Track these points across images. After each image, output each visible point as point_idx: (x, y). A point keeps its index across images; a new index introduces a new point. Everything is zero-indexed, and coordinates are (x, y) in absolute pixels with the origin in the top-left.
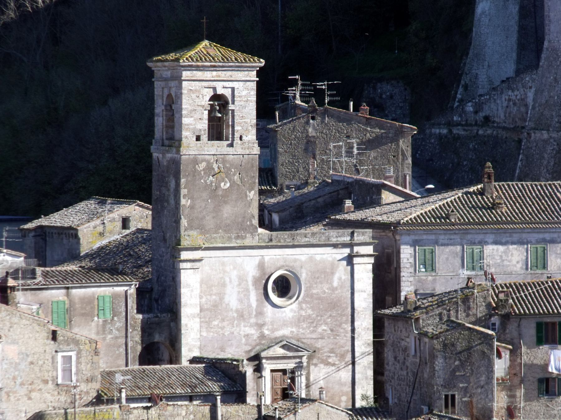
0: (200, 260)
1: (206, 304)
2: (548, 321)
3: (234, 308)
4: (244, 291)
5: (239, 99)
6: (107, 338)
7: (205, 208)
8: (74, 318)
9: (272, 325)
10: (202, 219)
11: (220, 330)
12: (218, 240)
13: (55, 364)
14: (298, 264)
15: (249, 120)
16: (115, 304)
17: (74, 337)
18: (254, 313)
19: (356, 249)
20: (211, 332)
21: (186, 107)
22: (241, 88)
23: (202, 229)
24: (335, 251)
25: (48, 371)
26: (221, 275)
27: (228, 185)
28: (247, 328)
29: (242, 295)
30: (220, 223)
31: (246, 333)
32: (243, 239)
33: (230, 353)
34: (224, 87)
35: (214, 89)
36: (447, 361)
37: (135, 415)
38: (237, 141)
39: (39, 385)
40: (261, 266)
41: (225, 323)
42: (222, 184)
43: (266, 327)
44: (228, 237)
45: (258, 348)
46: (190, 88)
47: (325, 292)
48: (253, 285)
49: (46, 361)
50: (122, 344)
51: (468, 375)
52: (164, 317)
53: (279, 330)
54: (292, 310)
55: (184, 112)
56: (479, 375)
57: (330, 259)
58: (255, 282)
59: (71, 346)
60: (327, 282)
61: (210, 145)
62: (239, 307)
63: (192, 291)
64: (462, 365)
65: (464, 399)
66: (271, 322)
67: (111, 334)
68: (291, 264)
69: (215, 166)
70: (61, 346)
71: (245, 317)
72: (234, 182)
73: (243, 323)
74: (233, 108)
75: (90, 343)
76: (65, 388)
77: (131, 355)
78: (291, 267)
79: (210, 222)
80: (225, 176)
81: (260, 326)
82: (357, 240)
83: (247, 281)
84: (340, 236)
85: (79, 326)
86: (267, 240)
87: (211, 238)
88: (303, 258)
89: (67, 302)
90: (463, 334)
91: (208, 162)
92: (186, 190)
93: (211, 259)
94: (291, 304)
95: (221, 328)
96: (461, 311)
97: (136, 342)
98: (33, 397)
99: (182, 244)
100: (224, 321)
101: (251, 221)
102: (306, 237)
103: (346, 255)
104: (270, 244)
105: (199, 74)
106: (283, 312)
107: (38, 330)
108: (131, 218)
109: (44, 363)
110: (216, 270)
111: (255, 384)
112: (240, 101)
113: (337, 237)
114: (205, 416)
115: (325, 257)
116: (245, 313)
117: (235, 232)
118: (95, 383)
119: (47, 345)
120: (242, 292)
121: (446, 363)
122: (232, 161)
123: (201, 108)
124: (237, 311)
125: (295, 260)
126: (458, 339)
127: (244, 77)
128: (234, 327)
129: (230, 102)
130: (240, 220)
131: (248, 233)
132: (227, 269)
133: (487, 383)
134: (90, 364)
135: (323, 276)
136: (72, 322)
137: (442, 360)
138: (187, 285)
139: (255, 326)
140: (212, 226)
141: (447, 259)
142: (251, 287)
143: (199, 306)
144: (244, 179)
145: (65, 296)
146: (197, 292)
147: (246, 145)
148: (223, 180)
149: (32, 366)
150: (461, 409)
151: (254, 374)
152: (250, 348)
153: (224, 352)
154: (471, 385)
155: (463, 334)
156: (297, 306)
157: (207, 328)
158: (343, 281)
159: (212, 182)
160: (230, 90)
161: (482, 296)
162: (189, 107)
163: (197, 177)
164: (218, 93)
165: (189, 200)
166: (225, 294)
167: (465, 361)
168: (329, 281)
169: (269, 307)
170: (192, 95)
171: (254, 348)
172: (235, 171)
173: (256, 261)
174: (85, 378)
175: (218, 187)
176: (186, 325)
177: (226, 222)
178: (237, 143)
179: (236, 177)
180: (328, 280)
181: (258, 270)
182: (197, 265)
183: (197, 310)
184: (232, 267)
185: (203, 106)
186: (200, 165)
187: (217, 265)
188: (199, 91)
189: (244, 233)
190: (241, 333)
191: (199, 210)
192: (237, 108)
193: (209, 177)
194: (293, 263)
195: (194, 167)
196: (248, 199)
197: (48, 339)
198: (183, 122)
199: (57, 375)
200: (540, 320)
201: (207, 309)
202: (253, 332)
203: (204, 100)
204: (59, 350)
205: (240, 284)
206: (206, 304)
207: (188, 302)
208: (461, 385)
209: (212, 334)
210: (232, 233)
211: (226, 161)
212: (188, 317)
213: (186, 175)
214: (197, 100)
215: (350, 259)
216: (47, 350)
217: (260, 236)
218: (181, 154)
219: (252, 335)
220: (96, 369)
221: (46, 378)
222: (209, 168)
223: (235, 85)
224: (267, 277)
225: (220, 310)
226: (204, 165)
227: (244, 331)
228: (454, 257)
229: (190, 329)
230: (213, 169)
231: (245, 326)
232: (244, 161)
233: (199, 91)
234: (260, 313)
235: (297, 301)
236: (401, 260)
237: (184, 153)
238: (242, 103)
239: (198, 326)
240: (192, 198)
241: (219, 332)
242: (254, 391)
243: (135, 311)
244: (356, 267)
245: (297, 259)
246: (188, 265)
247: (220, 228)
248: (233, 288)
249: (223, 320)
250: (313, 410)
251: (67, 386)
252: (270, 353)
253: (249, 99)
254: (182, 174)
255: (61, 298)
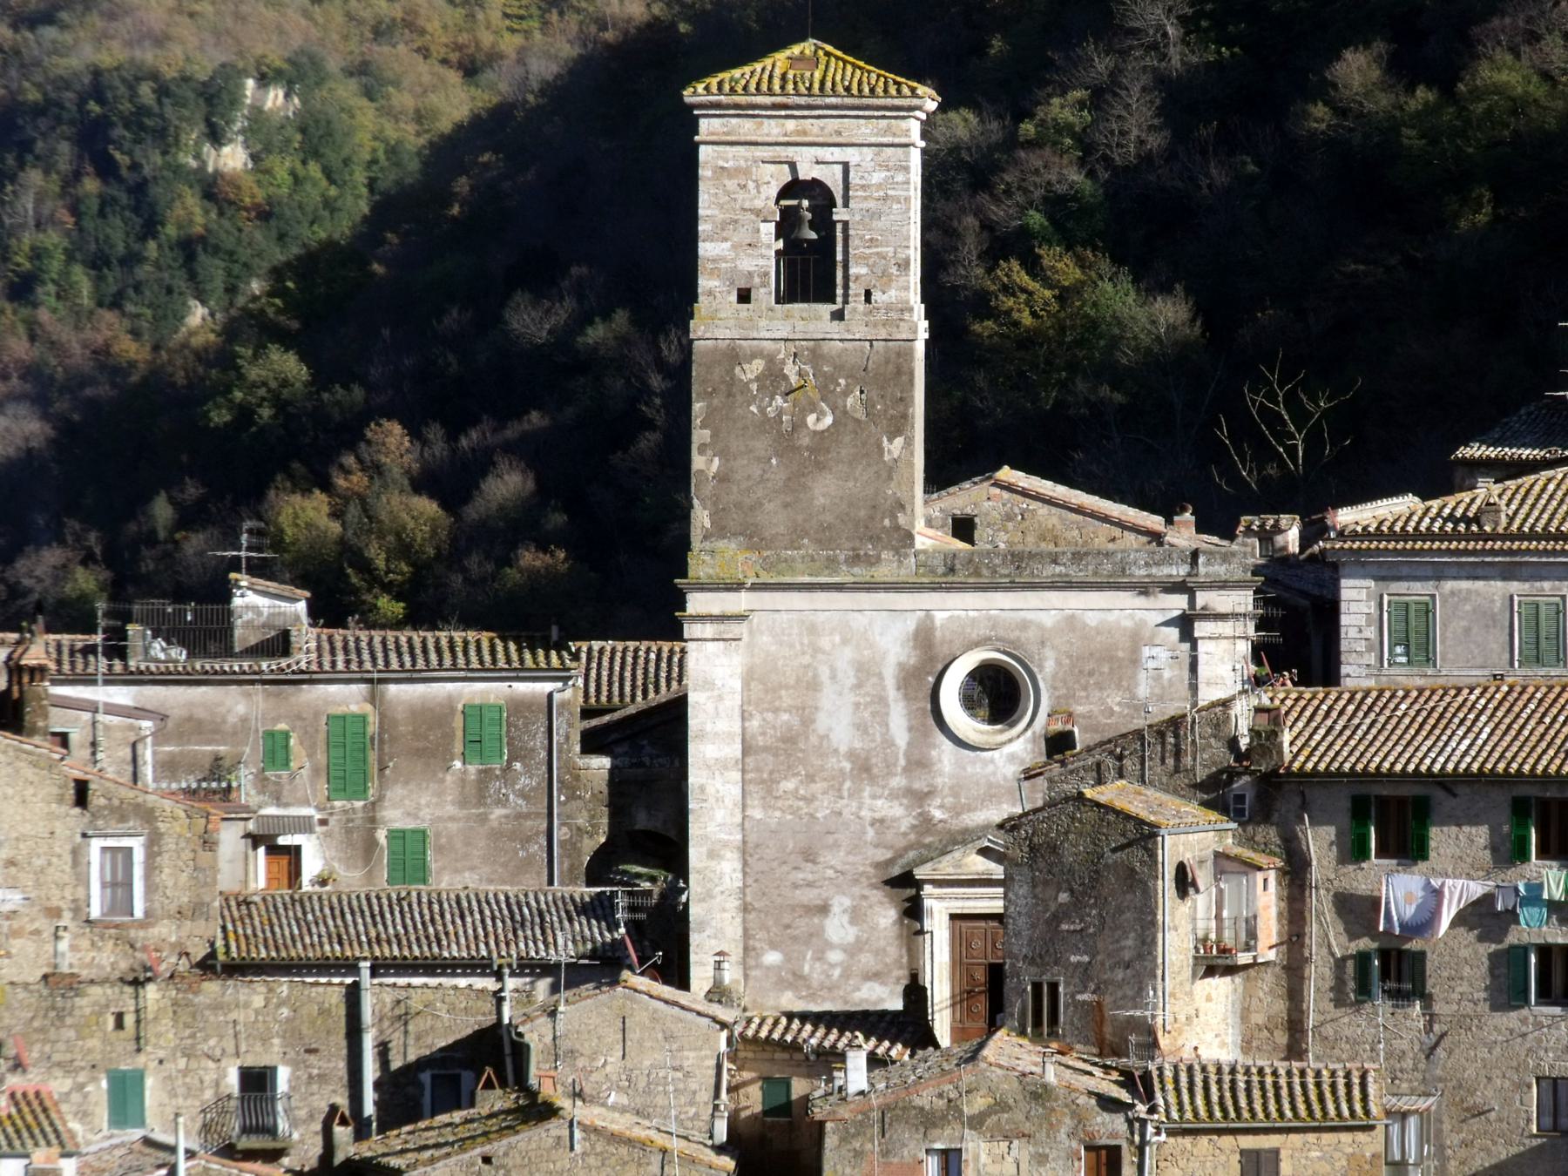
0: (740, 618)
1: (764, 734)
2: (1385, 793)
3: (843, 749)
4: (872, 702)
5: (860, 193)
6: (492, 817)
7: (762, 480)
8: (391, 759)
9: (956, 795)
10: (752, 508)
11: (801, 803)
12: (799, 566)
13: (82, 868)
14: (1032, 634)
15: (891, 249)
16: (516, 726)
17: (140, 800)
18: (902, 762)
19: (1202, 598)
20: (774, 808)
21: (709, 212)
22: (868, 165)
23: (754, 538)
24: (1141, 601)
25: (62, 886)
26: (806, 659)
27: (828, 420)
28: (879, 803)
29: (867, 715)
30: (805, 521)
31: (877, 815)
32: (872, 564)
33: (832, 867)
34: (818, 163)
35: (793, 166)
36: (1038, 890)
37: (92, 999)
38: (857, 304)
39: (32, 921)
40: (924, 638)
41: (818, 787)
42: (811, 419)
43: (938, 801)
44: (828, 558)
45: (912, 854)
46: (721, 163)
47: (1112, 713)
48: (899, 689)
49: (55, 860)
50: (537, 834)
51: (1091, 930)
52: (661, 766)
53: (975, 809)
54: (1012, 758)
55: (703, 227)
56: (1119, 932)
57: (1128, 623)
58: (904, 679)
59: (131, 824)
60: (1119, 686)
61: (779, 315)
62: (858, 745)
63: (720, 698)
64: (1078, 902)
65: (1080, 997)
66: (951, 788)
67: (504, 806)
68: (1013, 636)
69: (791, 370)
70: (100, 823)
71: (875, 771)
72: (845, 412)
73: (868, 788)
74: (846, 218)
75: (189, 817)
76: (113, 931)
77: (561, 863)
78: (1011, 642)
79: (774, 517)
80: (818, 396)
81: (920, 798)
82: (1207, 575)
83: (880, 676)
84: (1157, 564)
85: (407, 783)
86: (941, 570)
87: (779, 560)
88: (1048, 620)
89: (371, 719)
90: (1080, 821)
91: (770, 359)
92: (707, 432)
93: (777, 615)
94: (1010, 741)
95: (803, 798)
96: (1151, 759)
97: (579, 829)
98: (14, 951)
99: (691, 574)
100: (813, 781)
101: (894, 517)
102: (1055, 562)
103: (1177, 613)
104: (950, 579)
105: (745, 128)
106: (986, 763)
107: (31, 777)
108: (977, 520)
109: (50, 864)
110: (792, 646)
111: (904, 951)
112: (866, 198)
113: (1147, 564)
114: (329, 1011)
115: (1112, 617)
116: (874, 761)
117: (848, 545)
118: (203, 922)
119: (58, 818)
120: (867, 705)
121: (1035, 897)
122: (839, 356)
123: (753, 217)
124: (852, 755)
125: (1024, 625)
126: (1067, 833)
127: (877, 135)
128: (842, 798)
129: (839, 201)
130: (862, 513)
131: (884, 548)
132: (825, 643)
133: (1140, 957)
134: (189, 870)
135: (1106, 669)
136: (387, 772)
137: (1025, 887)
138: (706, 682)
139: (904, 796)
140: (782, 529)
141: (1467, 631)
142: (892, 693)
143: (739, 740)
144: (874, 406)
145: (366, 700)
146: (734, 701)
147: (881, 316)
148: (813, 408)
149: (13, 870)
150: (1072, 1024)
151: (902, 923)
152: (889, 855)
153: (814, 862)
154: (1099, 958)
155: (1080, 821)
156: (1029, 746)
157: (763, 798)
158: (1166, 683)
159: (780, 412)
160: (838, 169)
161: (1210, 723)
162: (716, 212)
163: (739, 398)
164: (801, 177)
165: (716, 460)
166: (816, 708)
167: (1084, 893)
168: (1125, 683)
169: (947, 745)
170: (726, 182)
171: (901, 856)
172: (847, 385)
173: (910, 623)
174: (173, 908)
175: (799, 425)
176: (702, 789)
177: (821, 518)
178: (855, 310)
179: (850, 401)
180: (1120, 680)
181: (915, 648)
182: (734, 629)
183: (736, 750)
184: (837, 639)
185: (757, 212)
186: (746, 366)
187: (796, 631)
188: (746, 172)
189: (874, 548)
190: (863, 813)
191: (744, 485)
192: (858, 218)
193: (772, 398)
194: (1017, 633)
195: (731, 372)
196: (887, 458)
197: (60, 800)
198: (701, 252)
199: (88, 896)
200: (1362, 790)
201: (766, 749)
202: (899, 814)
203: (763, 196)
204: (90, 833)
205: (859, 686)
206: (764, 734)
207: (709, 727)
208: (1073, 959)
209: (778, 814)
210: (839, 547)
211: (822, 356)
212: (709, 767)
213: (706, 392)
214: (741, 196)
215: (1185, 624)
216: (58, 831)
217: (922, 557)
218: (692, 336)
219: (895, 820)
220: (206, 884)
221: (55, 902)
222: (773, 377)
223: (850, 155)
224: (940, 667)
225: (802, 751)
226: (758, 366)
227: (872, 810)
228: (1487, 626)
229: (712, 800)
230: (786, 378)
231: (874, 797)
232: (874, 358)
233: (746, 172)
234: (919, 763)
235: (1029, 733)
236: (1343, 630)
237: (700, 334)
238: (871, 204)
239: (736, 791)
240: (724, 454)
241: (799, 808)
242: (901, 968)
243: (578, 748)
244: (1203, 647)
245: (1031, 622)
246: (708, 630)
247: (806, 534)
248: (840, 694)
249: (811, 778)
250: (610, 1008)
251: (117, 927)
252: (946, 867)
253: (890, 192)
254: (696, 389)
255: (354, 708)
